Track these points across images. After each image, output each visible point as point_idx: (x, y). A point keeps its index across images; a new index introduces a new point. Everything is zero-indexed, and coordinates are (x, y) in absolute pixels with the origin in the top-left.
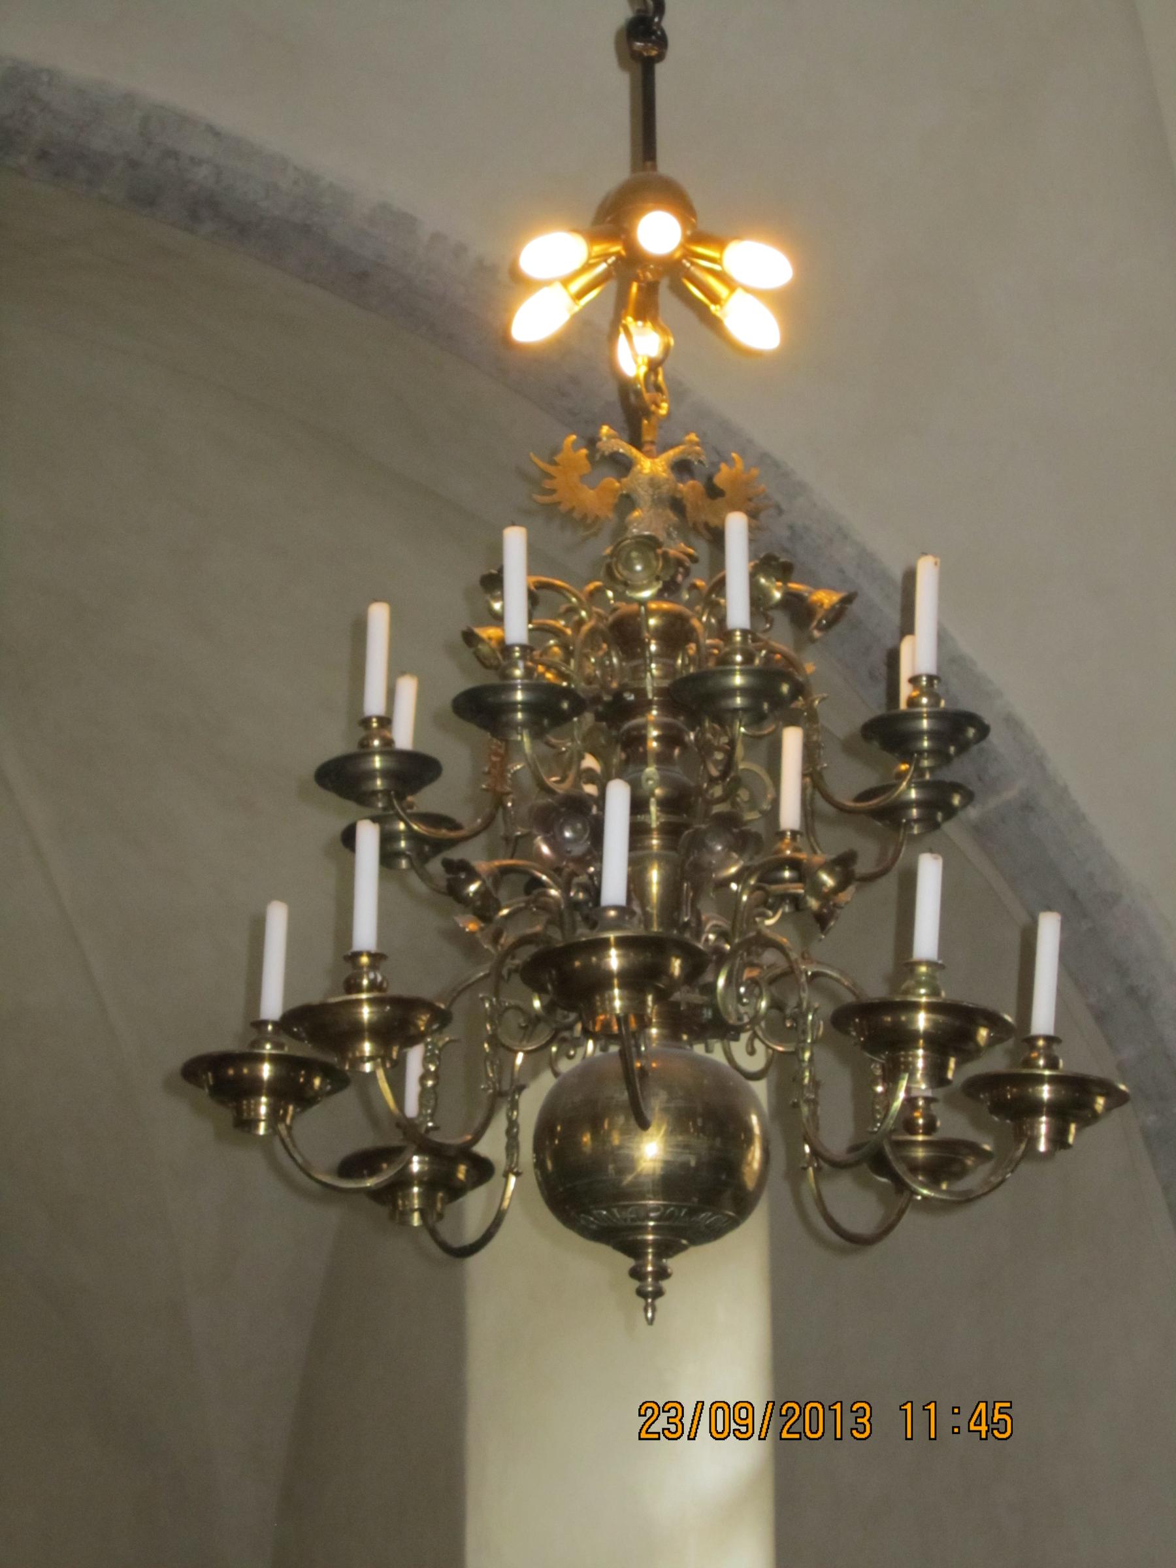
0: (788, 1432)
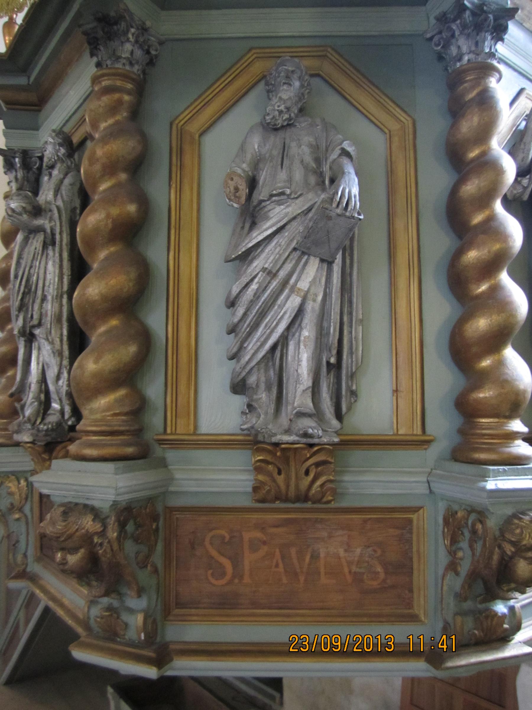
0: (357, 649)
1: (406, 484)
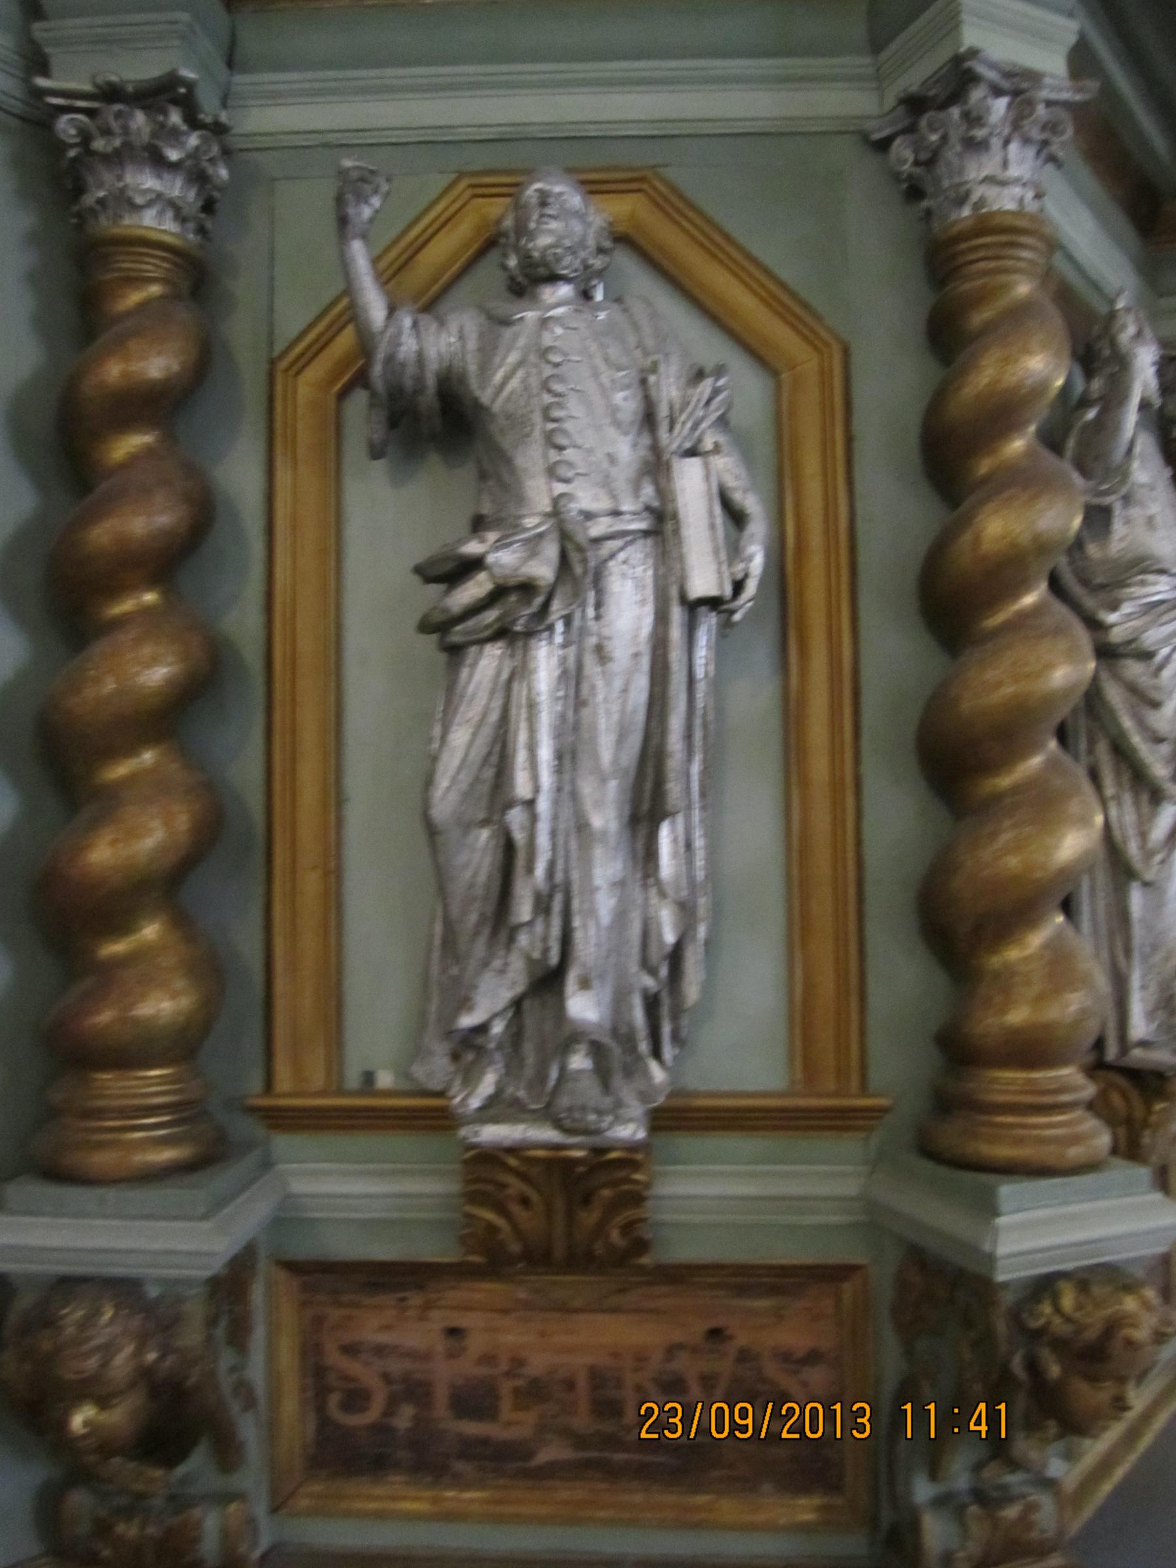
0: (647, 1432)
1: (1085, 1247)
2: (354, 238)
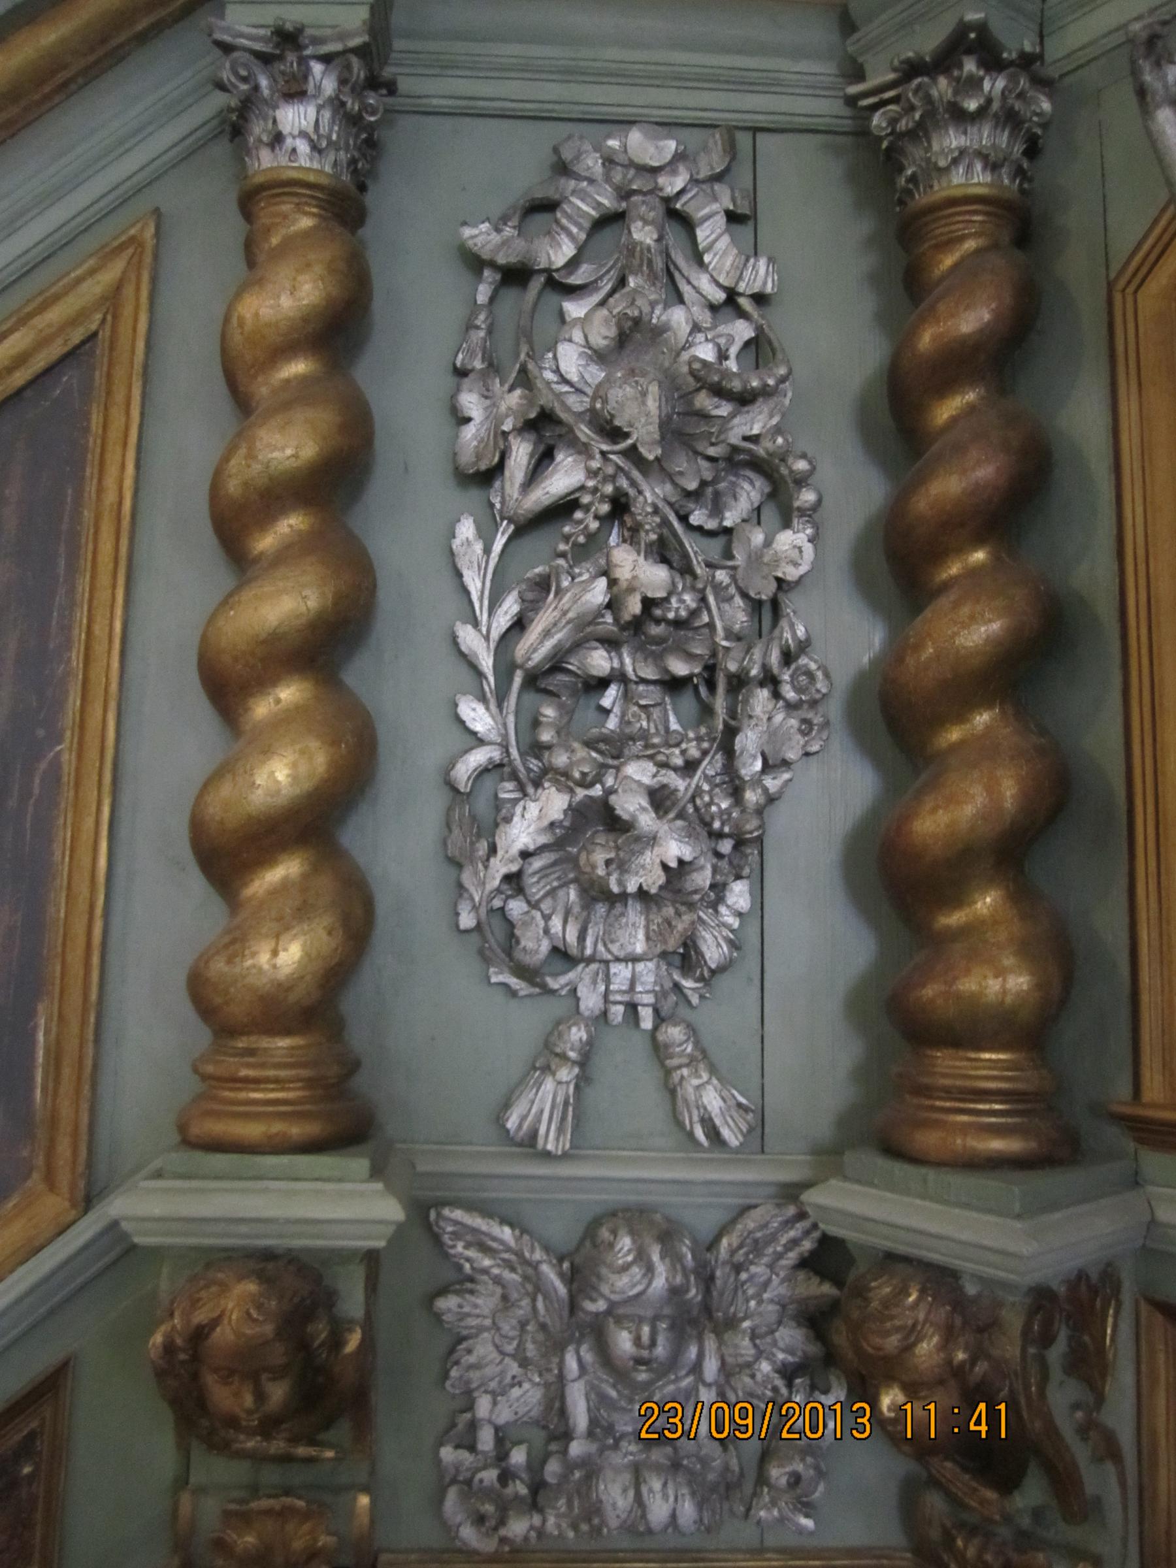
0: (788, 1432)
2: (1158, 107)
